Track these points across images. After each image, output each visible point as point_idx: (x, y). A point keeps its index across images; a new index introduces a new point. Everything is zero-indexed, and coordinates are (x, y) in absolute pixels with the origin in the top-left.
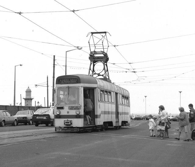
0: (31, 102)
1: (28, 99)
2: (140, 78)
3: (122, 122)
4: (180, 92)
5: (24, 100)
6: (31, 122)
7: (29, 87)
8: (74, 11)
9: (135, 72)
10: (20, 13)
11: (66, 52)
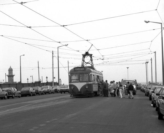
1: (11, 76)
6: (6, 96)
7: (10, 67)
11: (58, 47)
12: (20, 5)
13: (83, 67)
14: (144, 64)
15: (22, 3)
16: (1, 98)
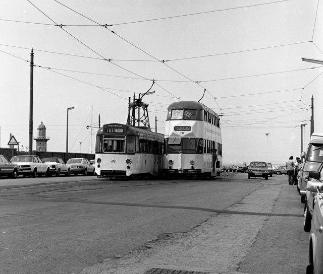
0: (46, 143)
12: (162, 63)
13: (126, 128)
14: (298, 127)
15: (163, 61)
16: (1, 227)
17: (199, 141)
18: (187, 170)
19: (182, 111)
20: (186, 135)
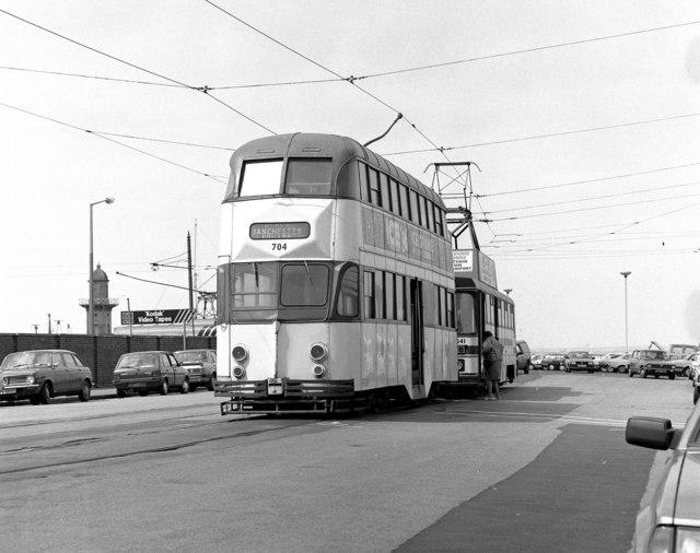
0: (109, 315)
1: (99, 306)
2: (499, 238)
3: (434, 384)
4: (626, 275)
5: (84, 309)
8: (351, 80)
9: (486, 221)
10: (205, 90)
17: (342, 272)
18: (298, 383)
19: (278, 167)
20: (294, 253)
